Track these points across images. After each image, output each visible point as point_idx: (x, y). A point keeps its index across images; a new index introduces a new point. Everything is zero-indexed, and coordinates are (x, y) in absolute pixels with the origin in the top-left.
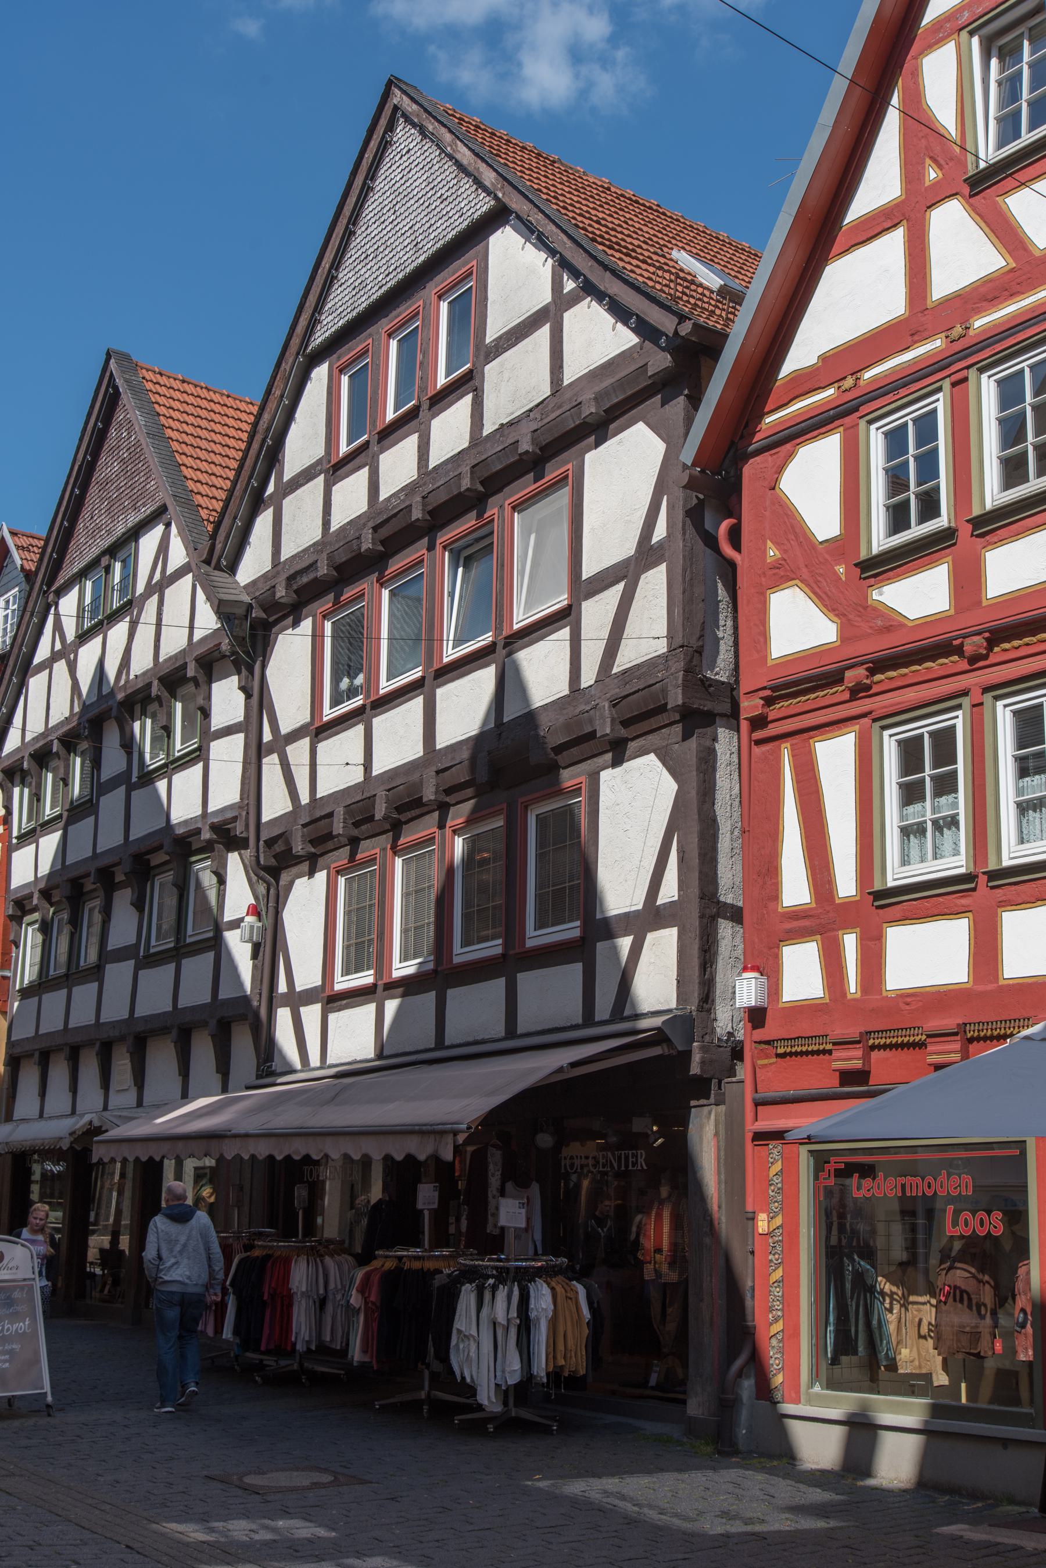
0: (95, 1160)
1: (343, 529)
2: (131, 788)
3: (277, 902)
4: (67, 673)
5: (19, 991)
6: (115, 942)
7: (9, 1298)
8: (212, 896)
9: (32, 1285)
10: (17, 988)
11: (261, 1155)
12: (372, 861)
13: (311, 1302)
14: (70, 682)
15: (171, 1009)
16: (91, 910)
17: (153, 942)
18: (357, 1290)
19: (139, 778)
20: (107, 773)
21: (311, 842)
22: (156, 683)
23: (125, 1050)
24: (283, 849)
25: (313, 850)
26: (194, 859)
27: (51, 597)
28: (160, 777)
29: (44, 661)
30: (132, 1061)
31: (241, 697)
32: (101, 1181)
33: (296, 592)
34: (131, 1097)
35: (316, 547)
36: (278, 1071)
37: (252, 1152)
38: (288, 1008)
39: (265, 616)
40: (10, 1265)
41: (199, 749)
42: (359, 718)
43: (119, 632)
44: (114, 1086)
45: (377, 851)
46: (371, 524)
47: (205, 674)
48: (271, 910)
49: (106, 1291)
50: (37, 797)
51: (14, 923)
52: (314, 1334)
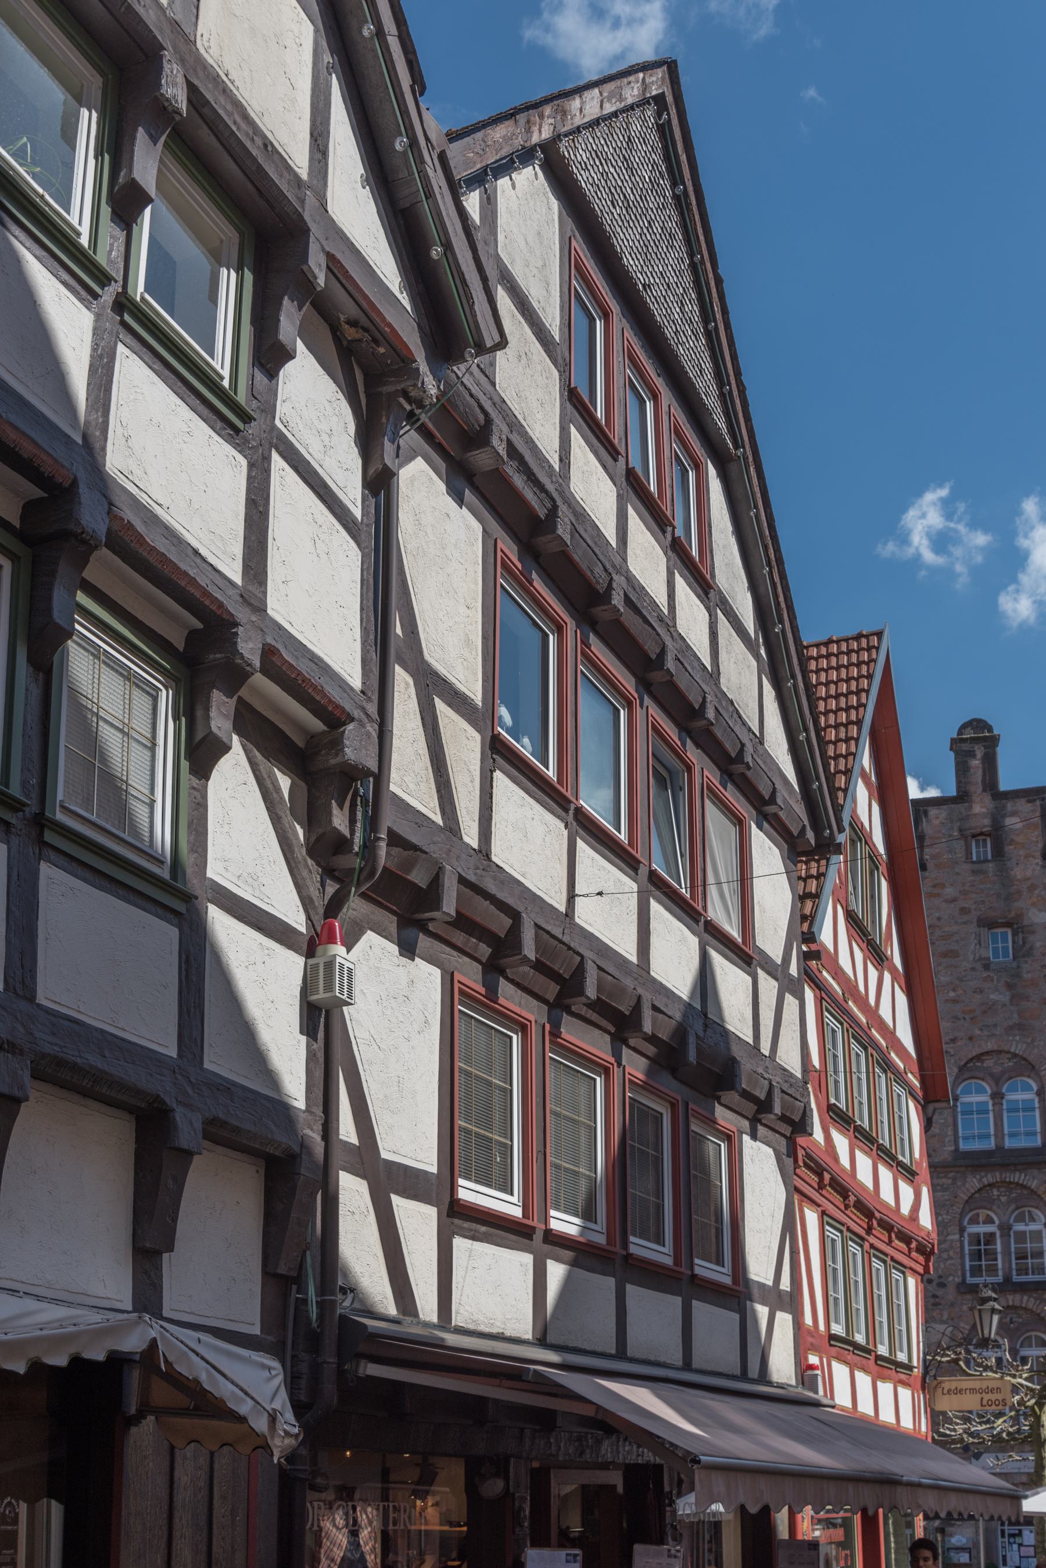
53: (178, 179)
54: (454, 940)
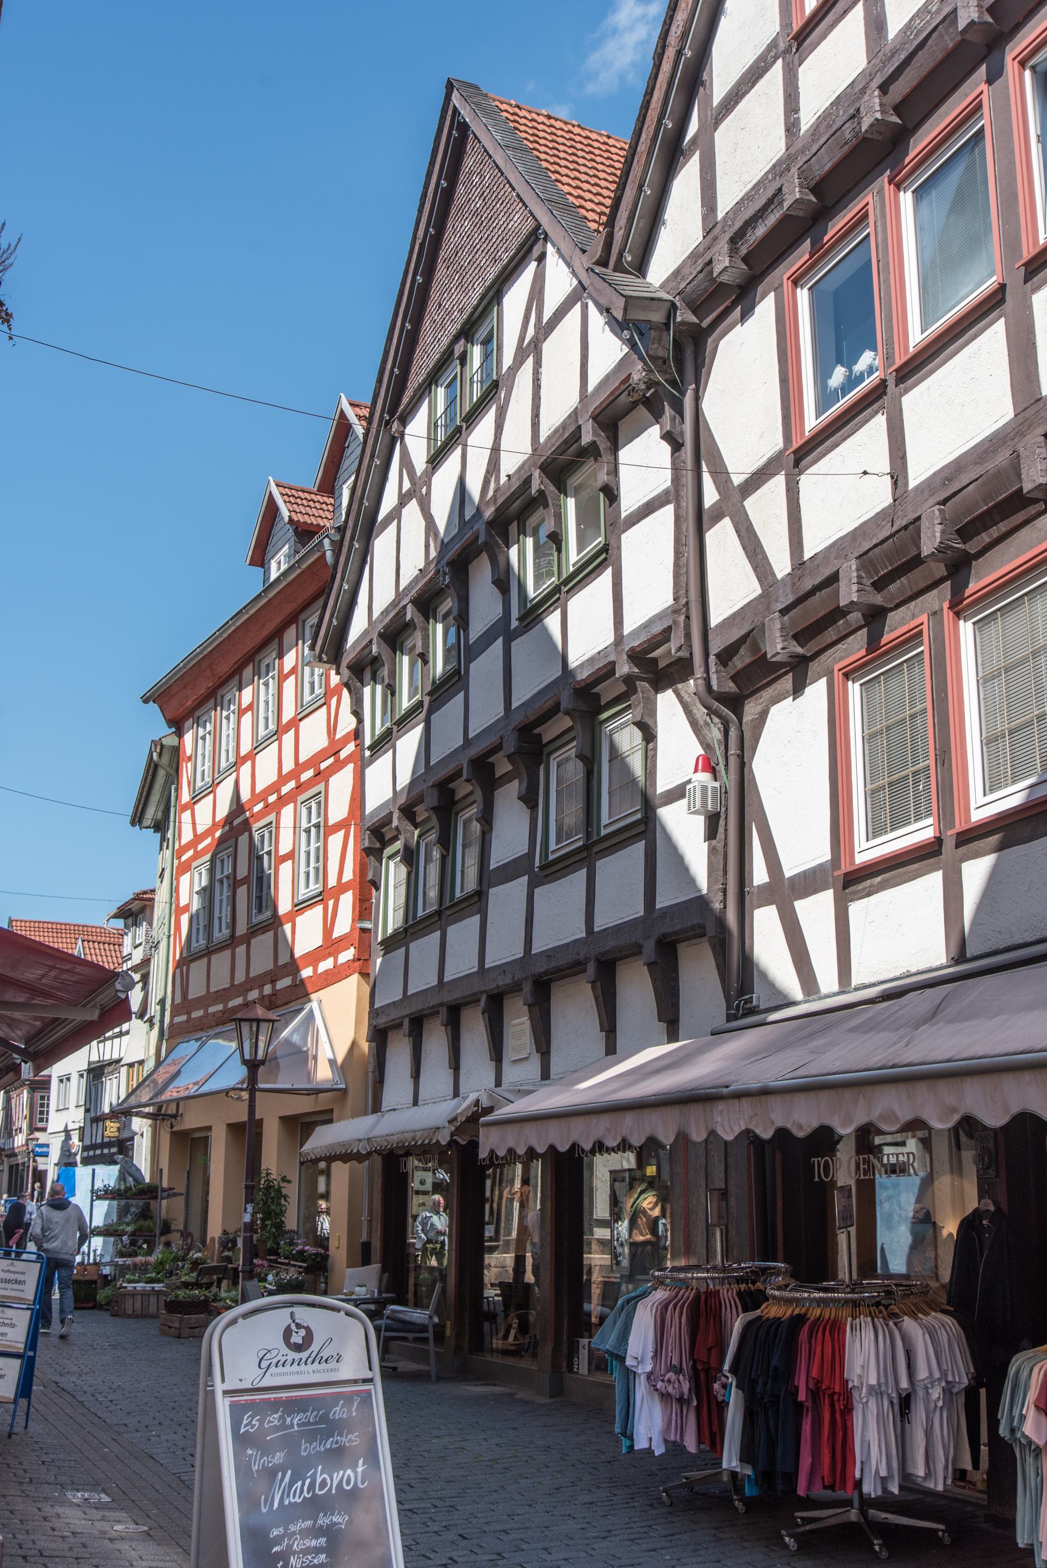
0: (483, 1154)
1: (825, 118)
2: (510, 637)
3: (742, 747)
4: (420, 513)
5: (381, 943)
6: (501, 854)
7: (324, 1419)
8: (637, 764)
9: (369, 1392)
10: (379, 939)
11: (800, 1127)
12: (914, 637)
13: (886, 1403)
14: (423, 523)
15: (584, 935)
16: (466, 823)
17: (553, 846)
18: (1037, 1407)
19: (521, 619)
20: (477, 629)
21: (795, 637)
22: (537, 473)
23: (521, 1002)
24: (748, 661)
25: (800, 650)
26: (605, 715)
27: (395, 426)
28: (548, 611)
29: (391, 512)
30: (531, 1018)
31: (666, 448)
32: (499, 1189)
33: (745, 260)
34: (533, 1068)
35: (779, 169)
36: (762, 1007)
37: (780, 1123)
38: (774, 907)
39: (696, 320)
40: (325, 1354)
41: (605, 549)
42: (875, 406)
43: (482, 433)
44: (509, 1055)
45: (924, 618)
46: (879, 80)
47: (608, 438)
48: (733, 761)
49: (511, 1338)
50: (391, 689)
51: (372, 858)
52: (895, 1465)
53: (580, 477)
54: (829, 641)
